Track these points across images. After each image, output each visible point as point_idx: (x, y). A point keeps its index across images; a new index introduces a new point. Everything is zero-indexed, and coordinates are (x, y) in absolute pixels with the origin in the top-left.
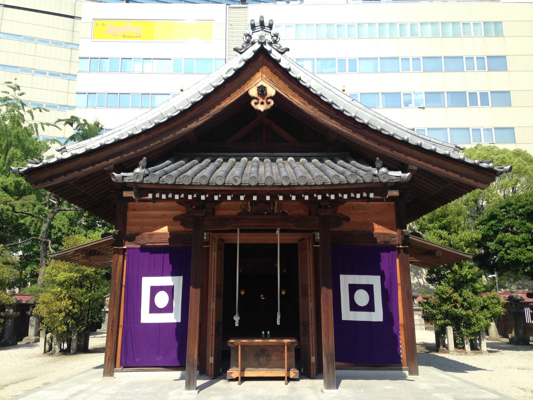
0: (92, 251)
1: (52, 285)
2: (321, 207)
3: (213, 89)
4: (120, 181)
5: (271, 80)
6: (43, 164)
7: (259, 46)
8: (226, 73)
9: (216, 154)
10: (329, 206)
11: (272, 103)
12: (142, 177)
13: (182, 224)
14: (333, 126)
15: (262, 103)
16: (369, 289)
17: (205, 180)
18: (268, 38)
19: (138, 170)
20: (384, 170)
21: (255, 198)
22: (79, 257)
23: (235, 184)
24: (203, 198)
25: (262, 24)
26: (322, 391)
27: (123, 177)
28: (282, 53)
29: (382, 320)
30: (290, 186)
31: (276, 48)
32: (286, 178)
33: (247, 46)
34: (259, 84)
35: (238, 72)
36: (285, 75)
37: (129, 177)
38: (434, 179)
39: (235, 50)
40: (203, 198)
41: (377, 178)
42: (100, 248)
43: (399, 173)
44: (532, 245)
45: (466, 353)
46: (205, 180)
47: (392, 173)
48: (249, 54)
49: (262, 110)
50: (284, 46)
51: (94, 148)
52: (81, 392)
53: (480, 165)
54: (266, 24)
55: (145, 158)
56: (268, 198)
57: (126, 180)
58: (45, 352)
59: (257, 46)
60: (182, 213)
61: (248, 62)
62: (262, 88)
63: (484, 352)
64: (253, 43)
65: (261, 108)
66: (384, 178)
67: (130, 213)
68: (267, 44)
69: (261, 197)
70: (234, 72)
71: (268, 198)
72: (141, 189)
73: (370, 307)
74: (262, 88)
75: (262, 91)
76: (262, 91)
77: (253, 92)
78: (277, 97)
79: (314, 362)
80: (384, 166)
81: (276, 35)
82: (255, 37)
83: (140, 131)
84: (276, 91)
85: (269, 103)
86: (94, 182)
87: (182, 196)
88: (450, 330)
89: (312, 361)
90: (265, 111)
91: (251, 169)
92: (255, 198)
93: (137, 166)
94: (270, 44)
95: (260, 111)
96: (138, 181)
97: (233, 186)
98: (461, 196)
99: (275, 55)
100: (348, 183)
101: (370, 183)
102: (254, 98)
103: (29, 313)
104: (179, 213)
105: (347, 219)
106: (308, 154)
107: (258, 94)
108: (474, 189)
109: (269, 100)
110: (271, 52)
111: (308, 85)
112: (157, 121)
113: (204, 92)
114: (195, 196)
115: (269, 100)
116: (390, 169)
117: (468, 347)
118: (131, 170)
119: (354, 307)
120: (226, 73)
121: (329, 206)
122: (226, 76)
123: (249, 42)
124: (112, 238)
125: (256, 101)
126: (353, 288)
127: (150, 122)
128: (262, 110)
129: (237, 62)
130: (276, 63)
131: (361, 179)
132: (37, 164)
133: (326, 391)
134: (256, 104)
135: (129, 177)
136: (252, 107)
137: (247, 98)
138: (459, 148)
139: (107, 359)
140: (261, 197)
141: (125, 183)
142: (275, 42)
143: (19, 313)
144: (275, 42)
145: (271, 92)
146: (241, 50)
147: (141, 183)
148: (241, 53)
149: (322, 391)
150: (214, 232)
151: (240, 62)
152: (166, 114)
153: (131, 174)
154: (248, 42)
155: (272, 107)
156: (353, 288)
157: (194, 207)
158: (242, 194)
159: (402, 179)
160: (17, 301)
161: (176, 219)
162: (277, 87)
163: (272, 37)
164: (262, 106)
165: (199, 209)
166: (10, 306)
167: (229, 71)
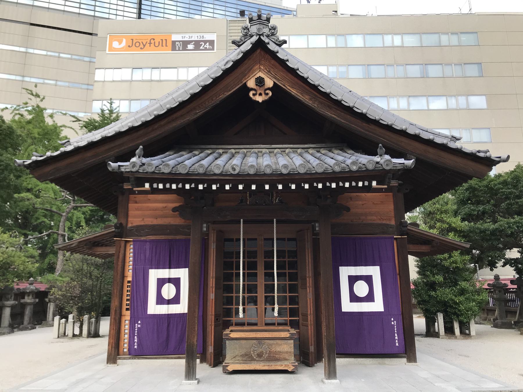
0: (95, 242)
1: (65, 274)
2: (320, 198)
3: (212, 80)
4: (116, 170)
5: (269, 72)
6: (47, 157)
7: (258, 37)
8: (225, 65)
9: (215, 146)
10: (329, 196)
11: (270, 94)
12: (138, 167)
13: (181, 215)
14: (332, 117)
15: (260, 94)
16: (368, 279)
17: (202, 169)
18: (266, 31)
19: (134, 160)
20: (387, 157)
21: (254, 187)
22: (84, 248)
23: (233, 173)
24: (201, 187)
25: (259, 17)
26: (322, 381)
27: (119, 166)
28: (280, 45)
29: (383, 311)
30: (289, 174)
31: (274, 40)
32: (285, 166)
33: (245, 39)
34: (258, 76)
35: (237, 64)
36: (282, 66)
37: (126, 166)
38: (435, 168)
39: (234, 42)
40: (201, 187)
41: (380, 165)
42: (103, 240)
43: (402, 161)
44: (1, 269)
45: (456, 338)
46: (202, 169)
47: (395, 160)
48: (247, 46)
49: (260, 101)
50: (281, 38)
51: (95, 140)
52: (82, 380)
53: (478, 154)
54: (264, 17)
55: (141, 147)
56: (267, 187)
57: (123, 169)
58: (58, 337)
59: (255, 39)
60: (181, 204)
61: (247, 55)
62: (260, 84)
63: (473, 336)
64: (252, 36)
65: (259, 99)
66: (387, 165)
67: (131, 206)
68: (265, 37)
69: (260, 186)
70: (232, 63)
71: (267, 187)
72: (139, 179)
73: (370, 298)
74: (260, 84)
75: (260, 82)
76: (260, 82)
77: (251, 83)
78: (275, 88)
79: (313, 351)
80: (386, 153)
81: (274, 28)
82: (254, 29)
83: (140, 123)
84: (274, 82)
85: (267, 94)
86: (95, 173)
87: (180, 186)
88: (440, 318)
89: (311, 351)
90: (263, 101)
91: (251, 160)
92: (254, 187)
93: (134, 155)
94: (268, 36)
95: (258, 102)
96: (134, 170)
97: (231, 175)
98: (460, 185)
99: (272, 47)
100: (351, 171)
101: (373, 170)
102: (252, 89)
103: (47, 300)
104: (177, 205)
105: (348, 209)
106: (306, 146)
107: (256, 85)
108: (471, 179)
109: (267, 91)
110: (269, 44)
111: (305, 76)
112: (156, 113)
113: (203, 84)
114: (193, 186)
115: (267, 91)
116: (393, 157)
117: (457, 331)
118: (128, 160)
119: (354, 298)
120: (225, 65)
121: (329, 196)
122: (224, 68)
123: (247, 35)
124: (114, 230)
125: (254, 92)
126: (353, 280)
127: (150, 114)
128: (260, 101)
129: (236, 54)
130: (273, 55)
131: (364, 166)
132: (41, 157)
133: (326, 381)
134: (254, 95)
135: (126, 166)
136: (251, 98)
137: (246, 89)
138: (455, 138)
139: (110, 346)
140: (260, 186)
141: (122, 172)
142: (273, 34)
143: (37, 300)
144: (273, 34)
145: (269, 83)
146: (239, 42)
147: (137, 172)
148: (239, 46)
149: (322, 381)
150: (214, 223)
151: (238, 54)
152: (165, 106)
153: (127, 163)
154: (245, 35)
155: (270, 98)
156: (353, 280)
157: (193, 198)
158: (241, 184)
159: (406, 166)
160: (36, 289)
161: (174, 210)
162: (275, 78)
163: (270, 29)
164: (261, 97)
165: (201, 200)
166: (29, 294)
167: (227, 63)
